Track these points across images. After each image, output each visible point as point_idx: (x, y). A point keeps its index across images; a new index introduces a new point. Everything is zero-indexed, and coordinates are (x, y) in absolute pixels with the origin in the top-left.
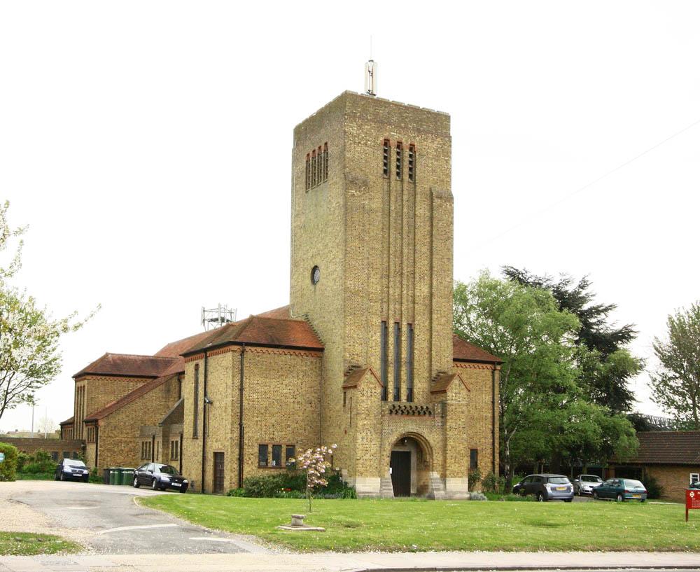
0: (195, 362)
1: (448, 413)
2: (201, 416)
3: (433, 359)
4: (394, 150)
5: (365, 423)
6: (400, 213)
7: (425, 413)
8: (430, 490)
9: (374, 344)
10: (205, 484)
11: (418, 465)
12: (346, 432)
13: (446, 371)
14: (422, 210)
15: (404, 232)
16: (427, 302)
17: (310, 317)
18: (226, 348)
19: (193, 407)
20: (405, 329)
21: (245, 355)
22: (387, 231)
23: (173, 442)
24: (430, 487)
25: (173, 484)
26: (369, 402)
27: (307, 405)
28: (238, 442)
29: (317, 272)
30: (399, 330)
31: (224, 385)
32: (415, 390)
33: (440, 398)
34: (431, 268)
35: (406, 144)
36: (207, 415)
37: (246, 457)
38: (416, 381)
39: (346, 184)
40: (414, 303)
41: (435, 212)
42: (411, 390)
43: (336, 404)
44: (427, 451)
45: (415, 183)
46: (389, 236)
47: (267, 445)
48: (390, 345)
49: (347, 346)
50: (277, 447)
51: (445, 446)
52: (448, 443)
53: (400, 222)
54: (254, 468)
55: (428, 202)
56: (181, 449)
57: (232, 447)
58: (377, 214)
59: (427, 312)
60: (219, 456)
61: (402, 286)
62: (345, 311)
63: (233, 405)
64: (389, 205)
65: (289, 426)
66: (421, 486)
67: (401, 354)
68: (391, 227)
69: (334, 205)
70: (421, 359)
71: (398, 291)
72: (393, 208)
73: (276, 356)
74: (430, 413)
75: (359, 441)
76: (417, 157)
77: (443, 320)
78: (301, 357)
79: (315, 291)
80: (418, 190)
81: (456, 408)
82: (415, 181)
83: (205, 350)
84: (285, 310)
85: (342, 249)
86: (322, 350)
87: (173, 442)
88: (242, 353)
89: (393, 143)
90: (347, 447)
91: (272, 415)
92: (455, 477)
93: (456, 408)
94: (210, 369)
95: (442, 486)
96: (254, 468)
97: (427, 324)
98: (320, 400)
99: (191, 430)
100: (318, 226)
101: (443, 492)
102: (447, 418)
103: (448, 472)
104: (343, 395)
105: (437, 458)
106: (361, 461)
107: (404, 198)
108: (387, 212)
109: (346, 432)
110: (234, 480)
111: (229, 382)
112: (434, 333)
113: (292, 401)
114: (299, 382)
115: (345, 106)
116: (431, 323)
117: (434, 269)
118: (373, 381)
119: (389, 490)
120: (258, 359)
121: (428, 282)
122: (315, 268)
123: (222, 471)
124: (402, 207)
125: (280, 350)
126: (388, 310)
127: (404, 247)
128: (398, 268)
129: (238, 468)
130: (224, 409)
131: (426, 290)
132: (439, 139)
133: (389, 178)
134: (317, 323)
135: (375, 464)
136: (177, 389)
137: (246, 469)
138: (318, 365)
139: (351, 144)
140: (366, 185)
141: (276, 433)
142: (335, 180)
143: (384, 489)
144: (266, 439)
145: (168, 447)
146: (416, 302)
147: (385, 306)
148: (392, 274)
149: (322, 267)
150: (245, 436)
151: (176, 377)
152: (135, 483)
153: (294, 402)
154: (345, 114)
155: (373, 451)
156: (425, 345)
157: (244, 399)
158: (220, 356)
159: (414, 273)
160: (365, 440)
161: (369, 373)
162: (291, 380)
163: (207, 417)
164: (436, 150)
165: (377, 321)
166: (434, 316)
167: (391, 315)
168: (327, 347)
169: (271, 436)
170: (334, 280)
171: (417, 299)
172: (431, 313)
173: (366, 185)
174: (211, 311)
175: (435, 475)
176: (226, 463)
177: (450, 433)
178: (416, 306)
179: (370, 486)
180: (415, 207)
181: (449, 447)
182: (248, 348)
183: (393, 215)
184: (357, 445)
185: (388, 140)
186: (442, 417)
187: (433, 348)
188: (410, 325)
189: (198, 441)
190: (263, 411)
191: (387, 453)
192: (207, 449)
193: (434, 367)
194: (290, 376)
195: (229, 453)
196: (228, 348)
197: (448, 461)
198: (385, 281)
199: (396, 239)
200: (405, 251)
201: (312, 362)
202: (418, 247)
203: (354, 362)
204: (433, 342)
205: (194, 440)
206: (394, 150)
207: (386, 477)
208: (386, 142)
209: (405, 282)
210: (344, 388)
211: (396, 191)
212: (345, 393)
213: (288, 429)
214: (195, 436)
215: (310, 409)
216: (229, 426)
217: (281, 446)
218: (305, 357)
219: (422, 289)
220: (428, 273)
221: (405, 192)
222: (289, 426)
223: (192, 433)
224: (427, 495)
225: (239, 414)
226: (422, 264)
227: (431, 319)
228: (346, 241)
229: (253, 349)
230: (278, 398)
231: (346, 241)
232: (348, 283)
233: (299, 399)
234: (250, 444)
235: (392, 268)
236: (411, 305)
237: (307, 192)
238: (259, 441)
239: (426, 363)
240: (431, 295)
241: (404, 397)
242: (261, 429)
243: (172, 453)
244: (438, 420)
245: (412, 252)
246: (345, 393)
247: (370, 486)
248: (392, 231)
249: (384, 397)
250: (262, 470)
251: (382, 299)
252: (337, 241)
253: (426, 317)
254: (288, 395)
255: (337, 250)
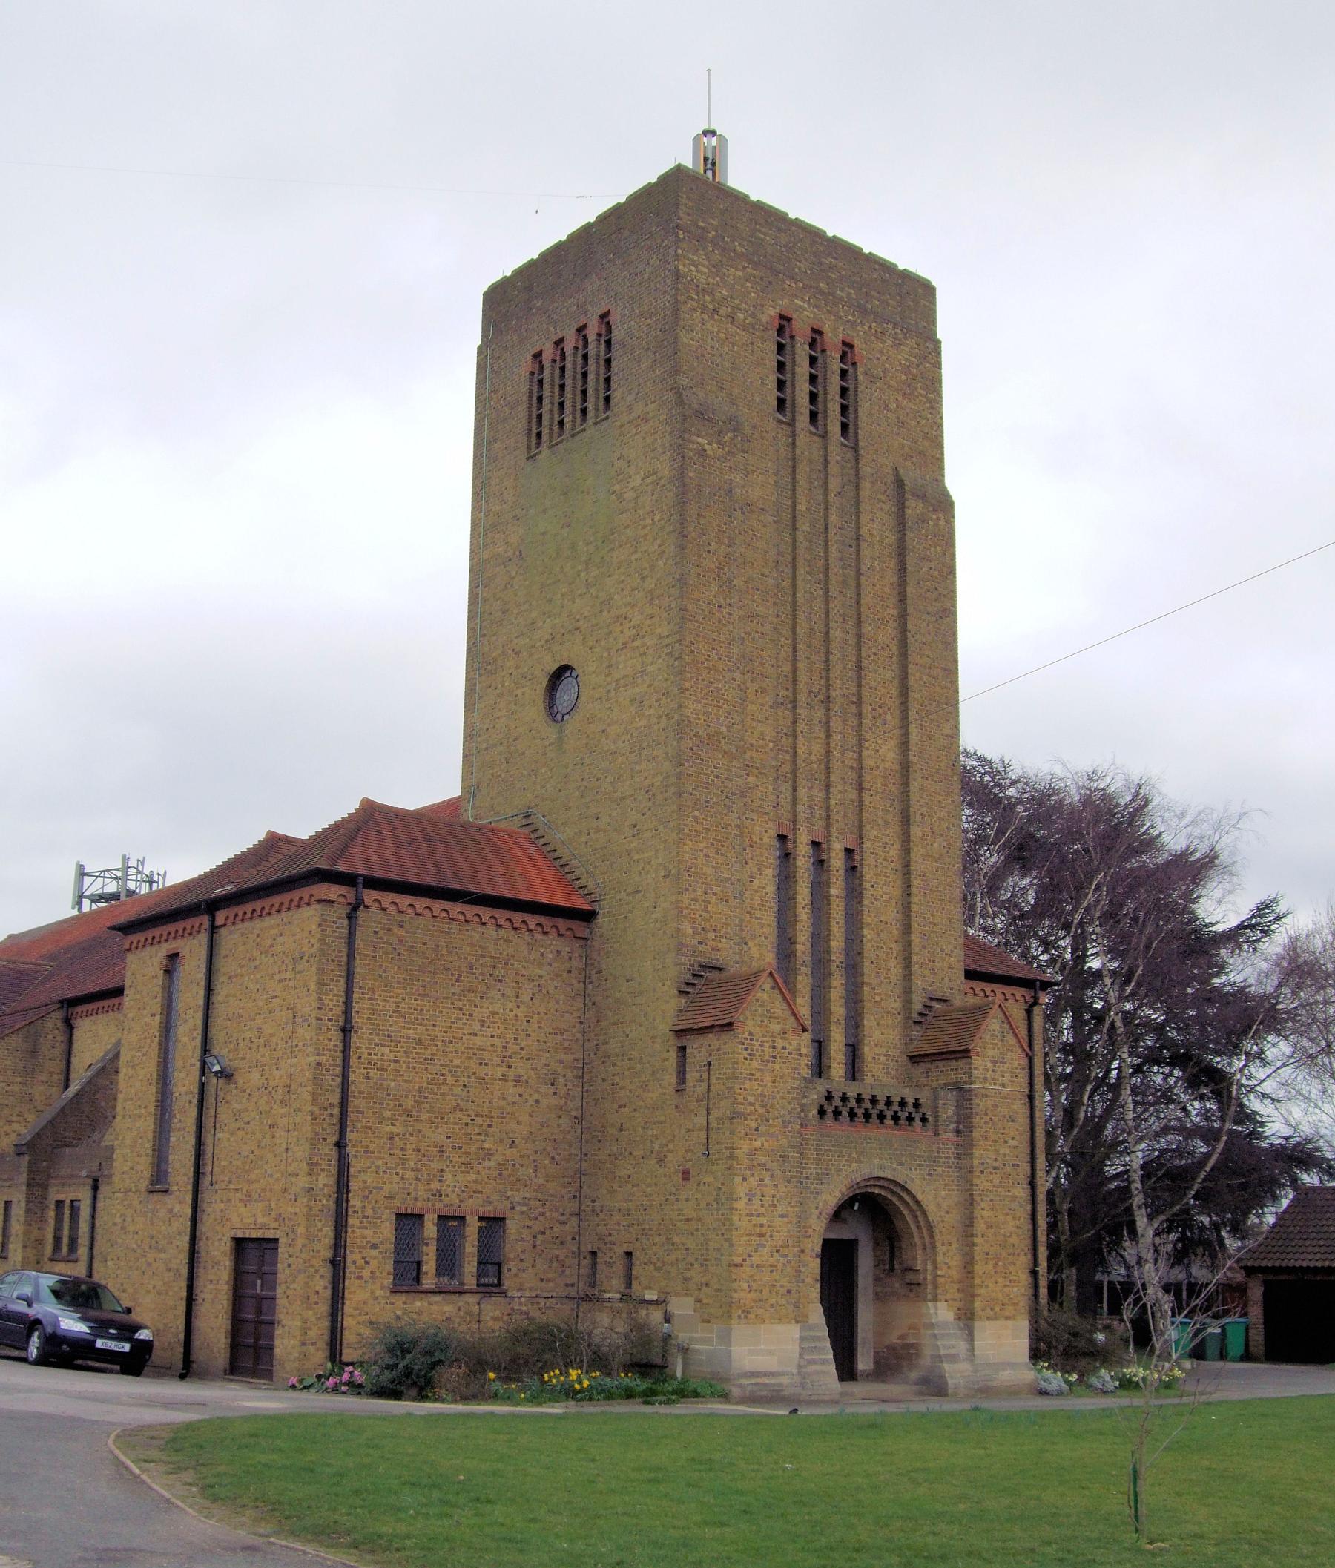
0: (165, 949)
1: (976, 1119)
2: (184, 1119)
3: (914, 958)
4: (802, 351)
5: (757, 1144)
6: (821, 527)
7: (910, 1119)
8: (926, 1361)
9: (757, 901)
10: (196, 1343)
11: (877, 1280)
12: (686, 1175)
13: (947, 996)
14: (877, 525)
15: (833, 580)
16: (894, 789)
17: (539, 820)
18: (295, 895)
19: (153, 1089)
20: (837, 862)
21: (361, 913)
22: (788, 571)
23: (59, 1204)
24: (927, 1352)
25: (100, 1343)
26: (768, 1078)
27: (544, 1088)
28: (332, 1205)
29: (567, 685)
30: (820, 863)
31: (284, 1015)
32: (866, 1049)
33: (947, 1072)
34: (904, 691)
35: (833, 337)
36: (210, 1112)
37: (353, 1257)
38: (869, 1022)
39: (685, 418)
40: (860, 788)
41: (910, 535)
42: (854, 1052)
43: (645, 1086)
44: (917, 1240)
45: (855, 448)
46: (794, 586)
47: (421, 1216)
48: (799, 910)
49: (686, 899)
50: (450, 1223)
51: (969, 1222)
52: (977, 1213)
53: (820, 551)
54: (379, 1293)
55: (889, 506)
56: (93, 1227)
57: (310, 1218)
58: (763, 518)
59: (894, 817)
60: (252, 1254)
61: (828, 736)
62: (680, 794)
63: (316, 1078)
64: (793, 498)
65: (489, 1154)
66: (892, 1348)
67: (828, 940)
68: (800, 561)
69: (637, 481)
70: (882, 955)
71: (818, 748)
72: (802, 507)
73: (454, 926)
74: (924, 1120)
75: (741, 1205)
76: (860, 378)
77: (937, 845)
78: (527, 936)
79: (560, 741)
80: (866, 469)
81: (995, 1106)
82: (857, 441)
83: (212, 906)
84: (452, 805)
85: (670, 609)
86: (587, 916)
87: (59, 1204)
88: (355, 909)
89: (801, 328)
90: (693, 1225)
91: (438, 1119)
92: (996, 1318)
93: (995, 1106)
94: (226, 966)
95: (961, 1346)
96: (379, 1293)
97: (894, 852)
98: (582, 1072)
99: (144, 1166)
100: (573, 547)
101: (964, 1366)
102: (975, 1134)
103: (978, 1304)
104: (673, 1055)
105: (948, 1257)
106: (747, 1270)
107: (831, 486)
108: (786, 516)
109: (686, 1175)
110: (313, 1334)
111: (307, 1006)
112: (916, 882)
113: (499, 1073)
114: (521, 1012)
115: (677, 206)
116: (906, 850)
117: (911, 695)
118: (779, 1012)
119: (823, 1362)
120: (401, 932)
121: (897, 732)
122: (560, 673)
123: (266, 1303)
124: (826, 509)
125: (466, 908)
126: (794, 801)
127: (833, 624)
128: (818, 683)
129: (328, 1293)
130: (279, 1095)
131: (889, 752)
132: (911, 342)
133: (792, 424)
134: (563, 836)
135: (784, 1281)
136: (60, 1048)
137: (356, 1294)
138: (575, 963)
139: (693, 309)
140: (736, 430)
141: (448, 1176)
142: (639, 409)
143: (811, 1362)
144: (418, 1200)
145: (43, 1220)
146: (866, 785)
147: (785, 788)
148: (802, 698)
149: (589, 671)
150: (354, 1185)
151: (59, 1015)
152: (33, 1352)
153: (504, 1079)
154: (678, 227)
155: (779, 1238)
156: (892, 914)
157: (354, 1062)
158: (267, 921)
159: (859, 702)
160: (756, 1201)
161: (767, 987)
162: (497, 1007)
163: (208, 1122)
164: (906, 370)
165: (765, 833)
166: (916, 831)
167: (800, 818)
168: (604, 909)
169: (435, 1185)
170: (640, 702)
171: (867, 776)
172: (906, 820)
173: (736, 430)
174: (100, 874)
175: (943, 1313)
176: (283, 1273)
177: (981, 1183)
178: (867, 799)
179: (771, 1353)
180: (858, 513)
181: (980, 1227)
182: (370, 896)
183: (804, 526)
184: (735, 1218)
185: (789, 320)
186: (958, 1132)
187: (914, 925)
188: (849, 852)
189: (169, 1201)
190: (409, 1103)
191: (815, 1245)
192: (205, 1227)
193: (918, 983)
194: (493, 993)
195: (300, 1242)
196: (305, 892)
197: (978, 1268)
198: (784, 715)
199: (844, 583)
200: (836, 634)
201: (559, 952)
202: (867, 628)
203: (707, 956)
204: (914, 908)
205: (156, 1197)
206: (802, 351)
207: (811, 1321)
208: (784, 322)
209: (836, 724)
210: (679, 1033)
211: (810, 461)
212: (682, 1049)
213: (486, 1163)
214: (159, 1182)
215: (553, 1101)
216: (301, 1151)
217: (462, 1219)
218: (539, 936)
219: (882, 753)
220: (894, 704)
221: (834, 468)
222: (489, 1154)
223: (147, 1174)
224: (914, 1375)
225: (336, 1111)
226: (881, 677)
227: (906, 838)
228: (682, 581)
229: (387, 898)
230: (457, 1062)
231: (682, 581)
232: (692, 707)
233: (521, 1069)
234: (369, 1212)
235: (803, 677)
236: (853, 795)
237: (530, 458)
238: (397, 1203)
239: (895, 970)
240: (905, 767)
241: (837, 1068)
242: (404, 1161)
243: (57, 1240)
244: (948, 1137)
245: (852, 641)
246: (682, 1049)
247: (771, 1353)
248: (801, 571)
249: (820, 1069)
250: (403, 1297)
251: (777, 769)
252: (650, 584)
253: (893, 832)
254: (486, 1055)
255: (648, 611)
